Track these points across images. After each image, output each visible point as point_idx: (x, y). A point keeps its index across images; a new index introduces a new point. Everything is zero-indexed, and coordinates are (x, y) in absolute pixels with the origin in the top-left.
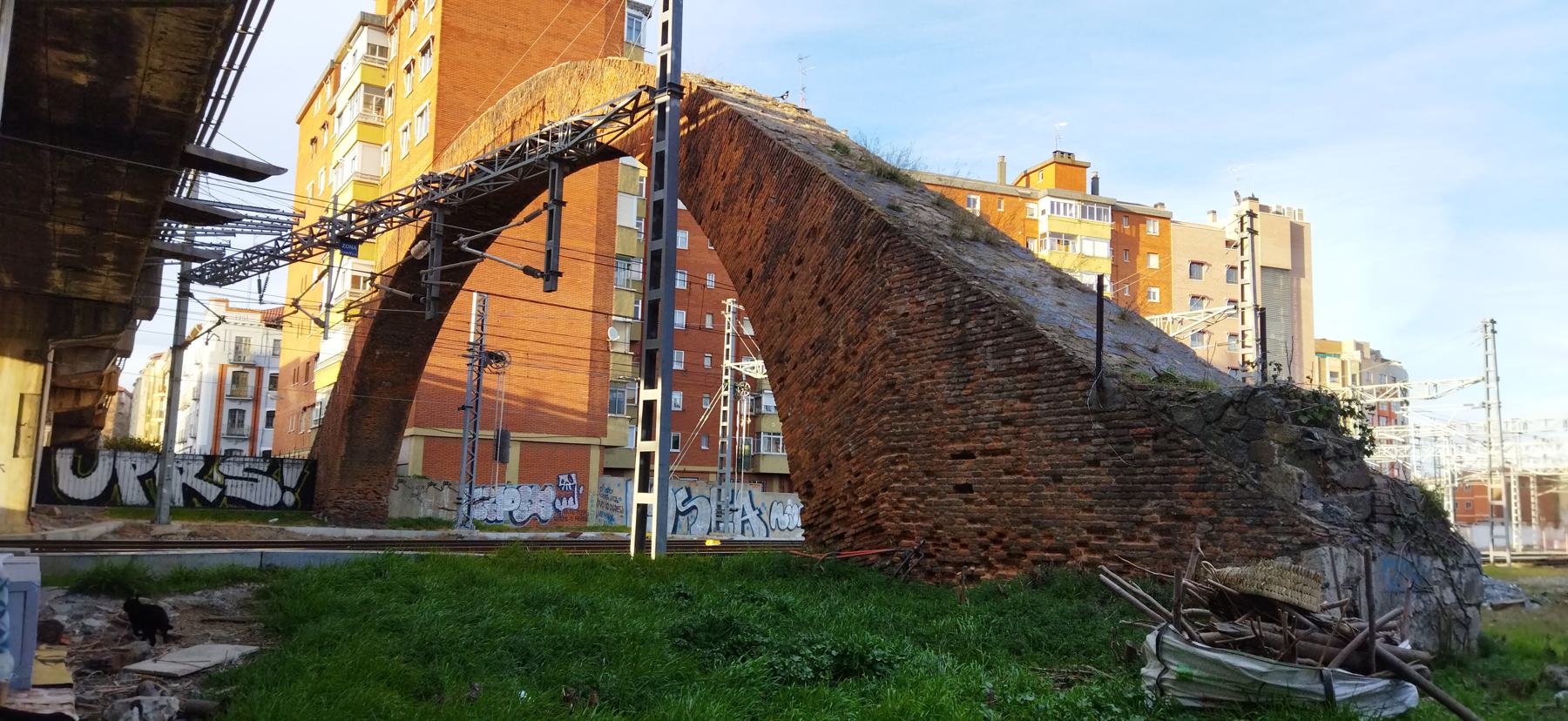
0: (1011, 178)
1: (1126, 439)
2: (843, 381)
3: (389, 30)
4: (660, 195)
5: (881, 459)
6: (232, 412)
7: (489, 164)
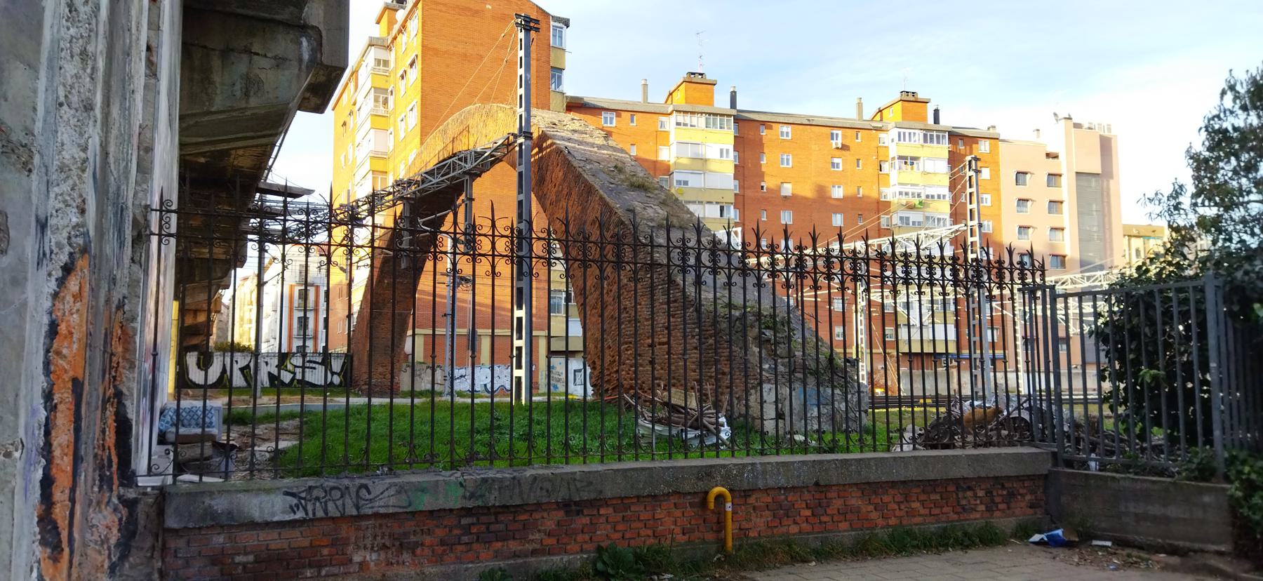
0: (868, 115)
3: (388, 48)
4: (522, 197)
7: (431, 173)
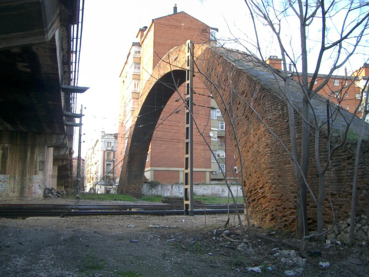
1: (339, 160)
2: (253, 145)
5: (265, 172)
6: (107, 165)
